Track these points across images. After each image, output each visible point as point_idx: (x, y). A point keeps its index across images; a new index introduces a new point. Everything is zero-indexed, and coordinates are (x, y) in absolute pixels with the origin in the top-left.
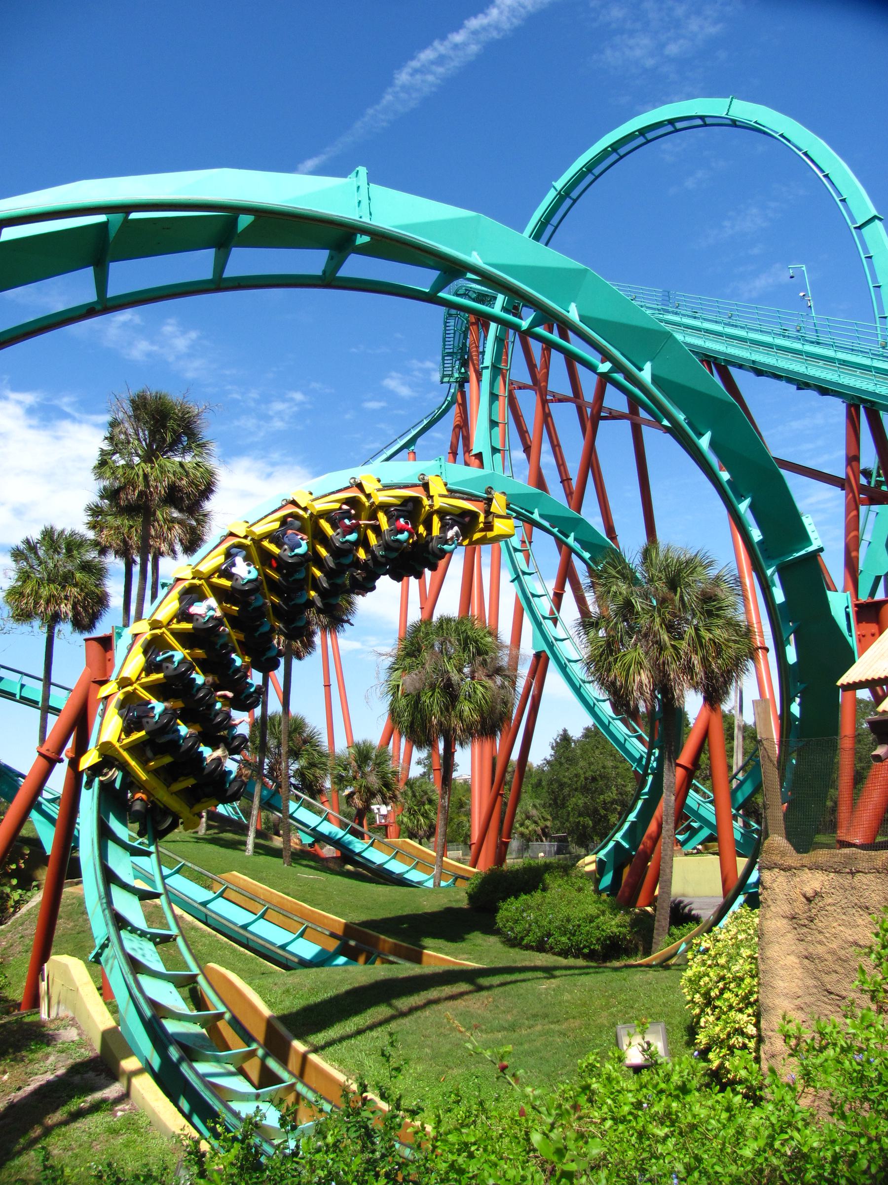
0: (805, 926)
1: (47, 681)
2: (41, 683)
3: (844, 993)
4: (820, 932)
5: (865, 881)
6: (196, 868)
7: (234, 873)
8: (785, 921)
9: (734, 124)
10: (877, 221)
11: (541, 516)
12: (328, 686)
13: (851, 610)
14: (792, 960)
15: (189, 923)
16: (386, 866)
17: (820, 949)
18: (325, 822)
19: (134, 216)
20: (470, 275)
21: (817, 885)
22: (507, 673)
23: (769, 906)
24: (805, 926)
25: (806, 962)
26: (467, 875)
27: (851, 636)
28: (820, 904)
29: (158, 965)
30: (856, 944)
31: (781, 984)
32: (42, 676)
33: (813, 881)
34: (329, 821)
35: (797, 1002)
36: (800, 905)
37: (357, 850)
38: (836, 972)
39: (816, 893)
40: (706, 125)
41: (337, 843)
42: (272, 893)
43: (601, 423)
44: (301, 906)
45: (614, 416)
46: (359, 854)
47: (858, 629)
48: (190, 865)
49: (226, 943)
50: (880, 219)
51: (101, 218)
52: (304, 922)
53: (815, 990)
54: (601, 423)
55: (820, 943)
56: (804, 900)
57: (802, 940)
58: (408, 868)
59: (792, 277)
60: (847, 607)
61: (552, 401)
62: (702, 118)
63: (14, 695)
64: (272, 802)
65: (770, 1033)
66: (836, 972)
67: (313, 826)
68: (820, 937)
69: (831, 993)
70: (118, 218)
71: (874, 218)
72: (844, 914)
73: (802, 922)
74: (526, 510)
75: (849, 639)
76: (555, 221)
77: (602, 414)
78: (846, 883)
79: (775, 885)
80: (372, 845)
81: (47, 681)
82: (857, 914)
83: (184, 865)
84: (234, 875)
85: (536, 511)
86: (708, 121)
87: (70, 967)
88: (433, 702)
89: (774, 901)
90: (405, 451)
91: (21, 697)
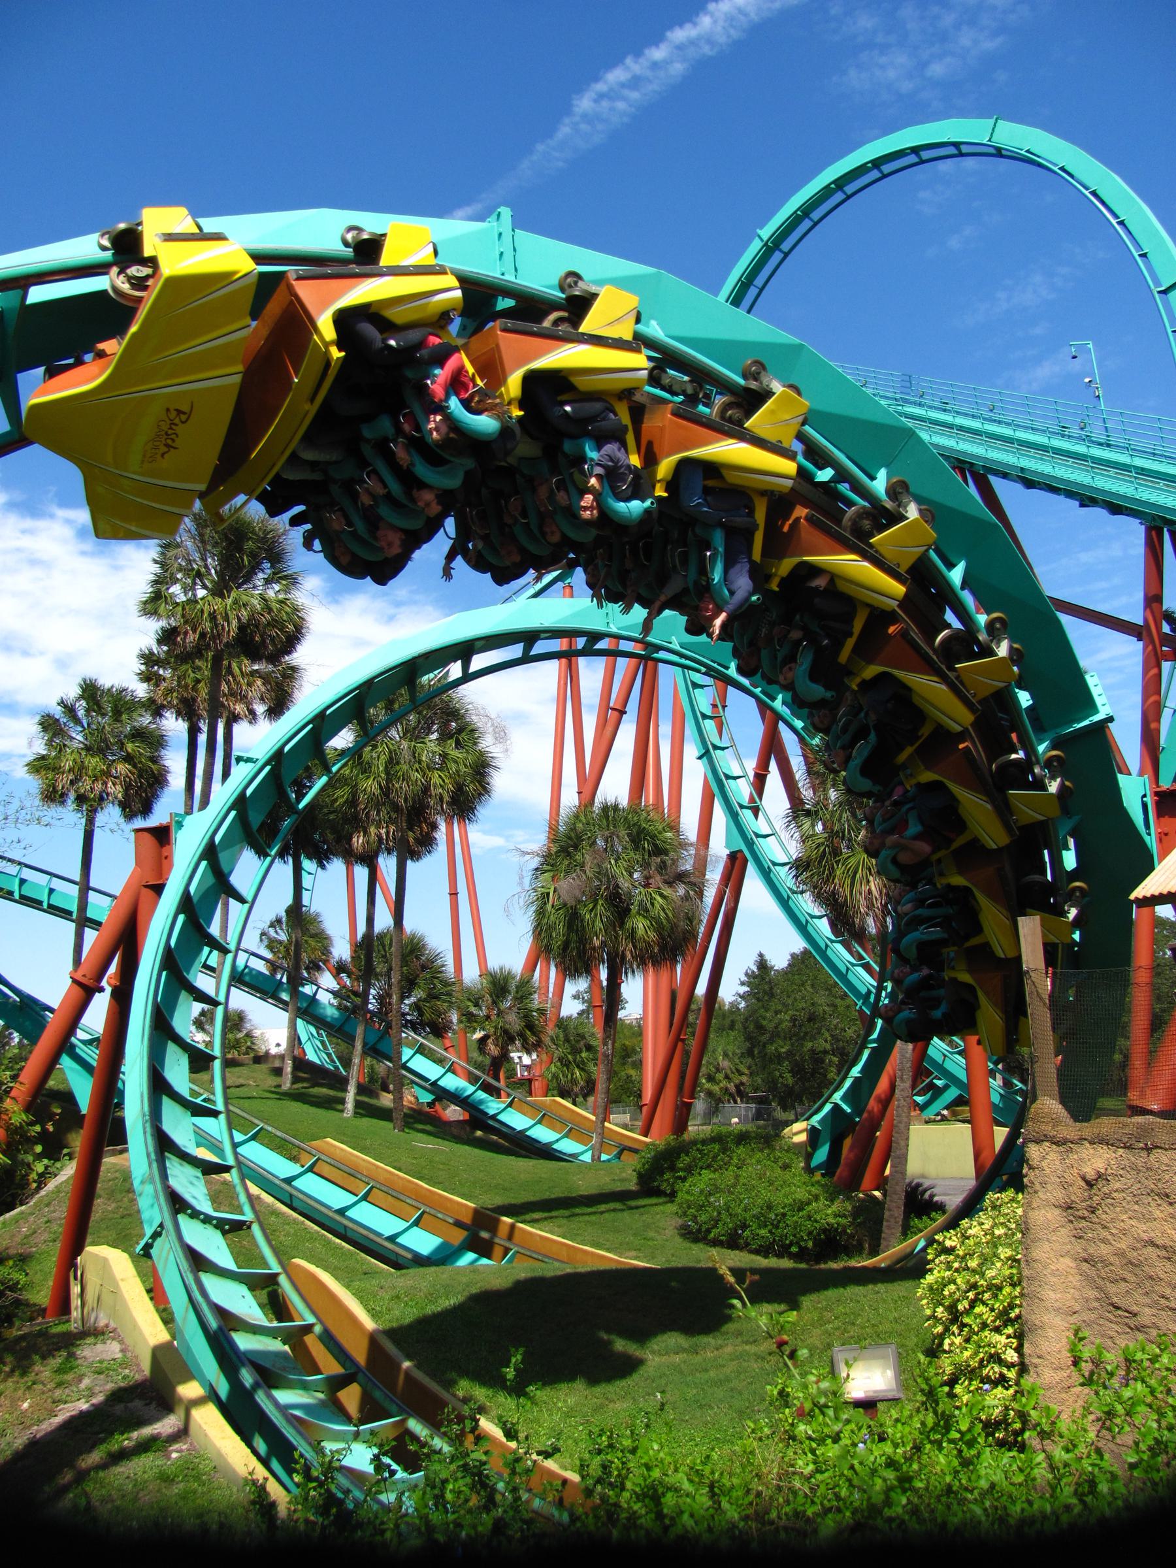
0: (1084, 1218)
2: (77, 887)
3: (1135, 1309)
4: (1104, 1227)
5: (1165, 1160)
6: (279, 1133)
8: (1058, 1212)
14: (1067, 1263)
17: (1105, 1250)
18: (449, 1074)
21: (1100, 1165)
22: (692, 879)
24: (1084, 1218)
25: (1085, 1266)
26: (636, 1146)
27: (1149, 834)
28: (1105, 1189)
31: (1052, 1294)
32: (77, 879)
33: (1096, 1159)
34: (454, 1072)
36: (1078, 1191)
37: (491, 1112)
38: (1124, 1280)
39: (1100, 1176)
40: (961, 155)
42: (378, 1167)
44: (416, 1184)
46: (494, 1117)
47: (1158, 824)
48: (270, 1129)
49: (317, 1232)
52: (419, 1205)
55: (1104, 1241)
56: (1082, 1183)
60: (1145, 796)
62: (956, 145)
63: (40, 903)
64: (382, 1047)
65: (1036, 1361)
66: (1124, 1280)
67: (433, 1079)
68: (1104, 1234)
69: (1118, 1308)
73: (1080, 1213)
74: (719, 664)
75: (1147, 838)
76: (759, 281)
78: (1140, 1162)
80: (510, 1105)
83: (262, 1129)
84: (328, 1143)
86: (964, 149)
88: (596, 918)
89: (1043, 1184)
90: (560, 584)
91: (50, 906)
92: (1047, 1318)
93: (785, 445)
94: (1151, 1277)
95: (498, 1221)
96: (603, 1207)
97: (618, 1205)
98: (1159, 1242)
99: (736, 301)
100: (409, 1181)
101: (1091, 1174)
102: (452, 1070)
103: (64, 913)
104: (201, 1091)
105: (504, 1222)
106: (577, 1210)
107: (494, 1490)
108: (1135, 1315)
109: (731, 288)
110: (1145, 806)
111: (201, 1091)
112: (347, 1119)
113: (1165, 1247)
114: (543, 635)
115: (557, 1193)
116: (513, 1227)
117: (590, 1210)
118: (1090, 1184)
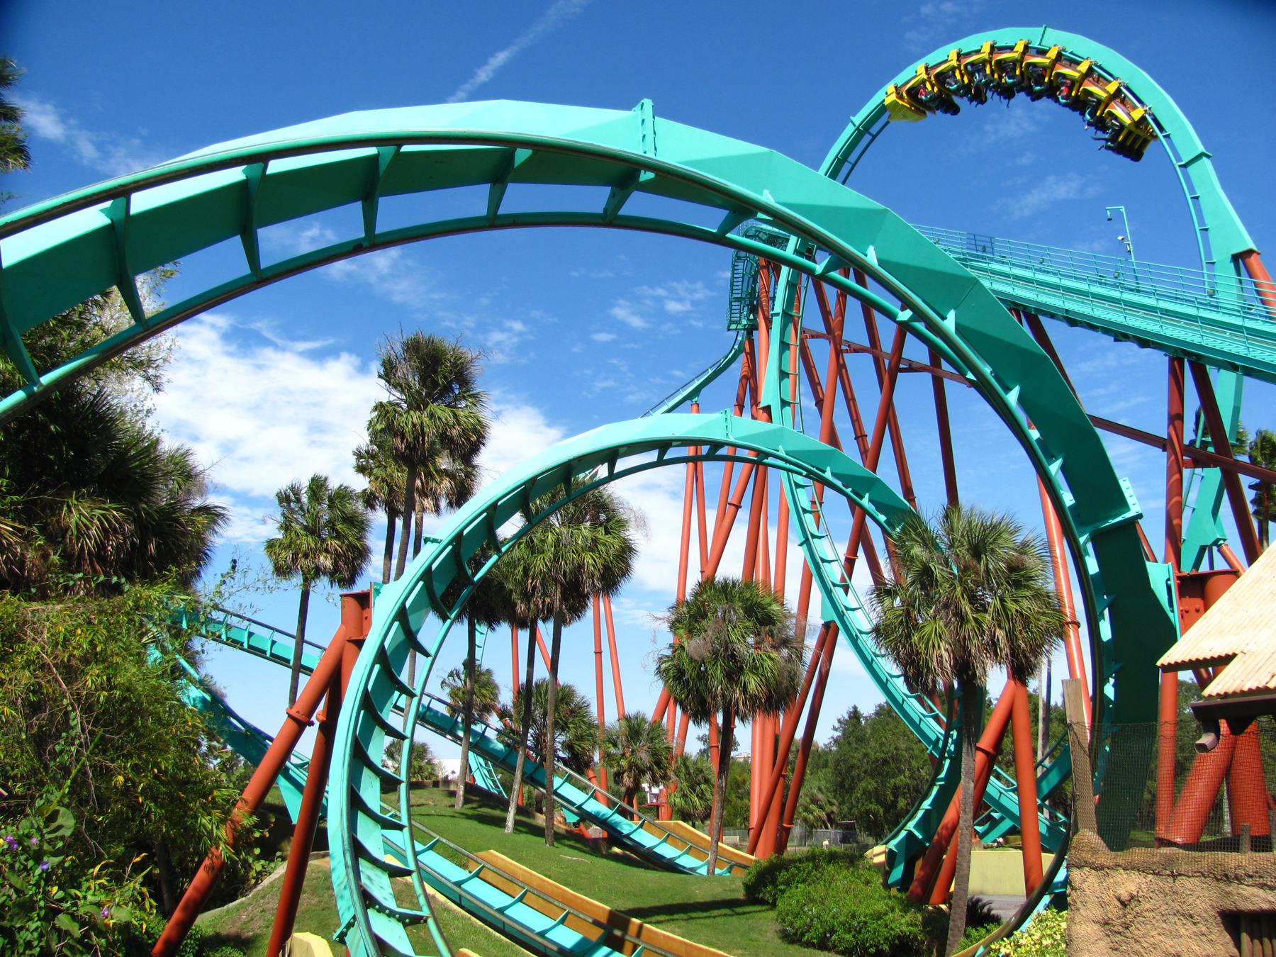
0: (1119, 933)
1: (301, 640)
2: (294, 641)
4: (1136, 941)
5: (1189, 885)
6: (452, 845)
7: (492, 851)
8: (1096, 927)
10: (1204, 158)
11: (833, 474)
12: (598, 653)
13: (1172, 583)
15: (442, 903)
16: (655, 850)
18: (592, 800)
19: (406, 148)
20: (760, 215)
21: (1133, 888)
22: (795, 645)
24: (1119, 933)
29: (391, 904)
33: (1129, 883)
34: (596, 798)
36: (1114, 910)
37: (625, 832)
39: (1132, 897)
41: (603, 822)
42: (531, 874)
44: (563, 890)
45: (913, 368)
46: (628, 836)
48: (444, 841)
49: (481, 927)
50: (1208, 157)
51: (372, 151)
56: (1118, 903)
58: (680, 853)
59: (1110, 220)
60: (1169, 579)
63: (264, 652)
67: (578, 804)
68: (1137, 947)
70: (389, 150)
73: (1116, 929)
74: (817, 469)
75: (1171, 615)
76: (852, 158)
78: (1167, 887)
79: (1085, 886)
81: (301, 640)
83: (438, 840)
84: (491, 854)
85: (828, 469)
89: (1084, 903)
90: (688, 402)
95: (629, 921)
96: (715, 912)
97: (727, 911)
100: (556, 887)
102: (594, 796)
103: (282, 661)
104: (390, 808)
105: (634, 923)
106: (694, 915)
111: (390, 808)
112: (508, 835)
115: (678, 900)
116: (641, 926)
117: (705, 914)
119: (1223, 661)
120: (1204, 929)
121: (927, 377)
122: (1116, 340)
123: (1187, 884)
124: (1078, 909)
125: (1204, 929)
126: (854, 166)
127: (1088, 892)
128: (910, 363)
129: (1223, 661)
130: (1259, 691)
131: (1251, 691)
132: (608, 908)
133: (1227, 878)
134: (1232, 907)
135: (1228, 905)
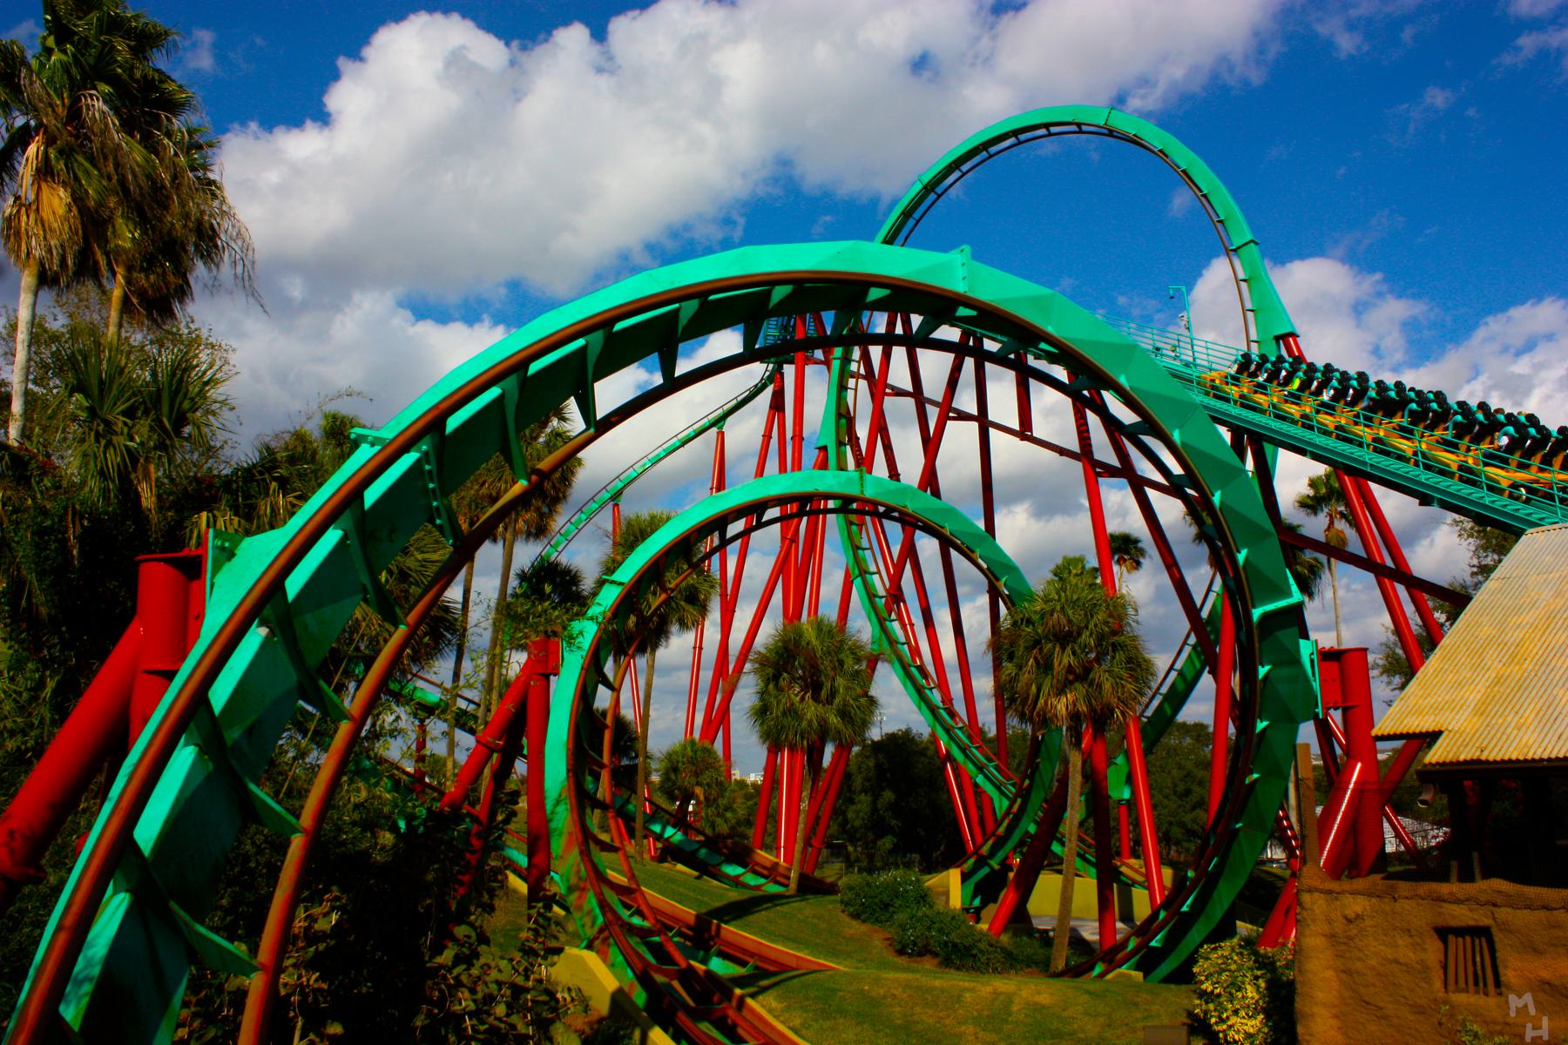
0: (1344, 943)
3: (1382, 1004)
4: (1360, 950)
5: (1407, 907)
8: (1323, 939)
9: (1111, 133)
10: (1252, 245)
13: (1315, 657)
14: (1329, 974)
17: (1359, 965)
20: (1043, 346)
21: (1359, 909)
23: (1308, 925)
24: (1344, 943)
25: (1343, 976)
28: (1362, 925)
30: (1397, 962)
31: (1320, 994)
33: (1357, 905)
35: (1334, 1011)
36: (1339, 926)
38: (1374, 985)
39: (1358, 916)
40: (1081, 132)
43: (949, 423)
45: (963, 416)
50: (1256, 244)
53: (1350, 1001)
54: (949, 423)
55: (1359, 959)
56: (1344, 921)
57: (1341, 956)
59: (1172, 298)
60: (1312, 654)
61: (889, 395)
62: (1079, 125)
65: (1308, 1038)
66: (1374, 985)
68: (1361, 955)
69: (1367, 1003)
71: (1251, 241)
72: (1385, 935)
73: (1341, 940)
75: (1314, 684)
76: (917, 215)
77: (951, 414)
78: (1387, 908)
79: (1315, 907)
82: (1398, 936)
86: (1084, 128)
87: (1471, 884)
89: (1314, 920)
92: (1316, 1010)
93: (598, 848)
94: (1395, 984)
98: (1402, 960)
99: (783, 469)
101: (1350, 913)
107: (125, 278)
108: (1381, 1008)
109: (889, 227)
110: (1312, 661)
113: (1406, 965)
114: (770, 504)
118: (1349, 921)
119: (1434, 736)
120: (1419, 940)
121: (974, 426)
122: (1421, 504)
123: (1404, 906)
124: (1308, 925)
125: (1419, 940)
126: (918, 222)
127: (1317, 912)
128: (893, 388)
129: (1434, 736)
130: (1472, 761)
131: (1465, 762)
132: (694, 912)
133: (1439, 899)
134: (1444, 924)
135: (1441, 922)
